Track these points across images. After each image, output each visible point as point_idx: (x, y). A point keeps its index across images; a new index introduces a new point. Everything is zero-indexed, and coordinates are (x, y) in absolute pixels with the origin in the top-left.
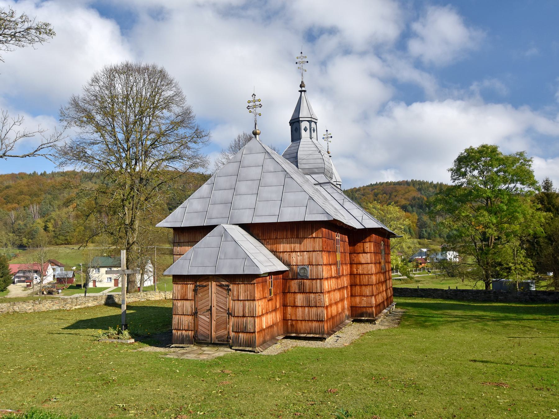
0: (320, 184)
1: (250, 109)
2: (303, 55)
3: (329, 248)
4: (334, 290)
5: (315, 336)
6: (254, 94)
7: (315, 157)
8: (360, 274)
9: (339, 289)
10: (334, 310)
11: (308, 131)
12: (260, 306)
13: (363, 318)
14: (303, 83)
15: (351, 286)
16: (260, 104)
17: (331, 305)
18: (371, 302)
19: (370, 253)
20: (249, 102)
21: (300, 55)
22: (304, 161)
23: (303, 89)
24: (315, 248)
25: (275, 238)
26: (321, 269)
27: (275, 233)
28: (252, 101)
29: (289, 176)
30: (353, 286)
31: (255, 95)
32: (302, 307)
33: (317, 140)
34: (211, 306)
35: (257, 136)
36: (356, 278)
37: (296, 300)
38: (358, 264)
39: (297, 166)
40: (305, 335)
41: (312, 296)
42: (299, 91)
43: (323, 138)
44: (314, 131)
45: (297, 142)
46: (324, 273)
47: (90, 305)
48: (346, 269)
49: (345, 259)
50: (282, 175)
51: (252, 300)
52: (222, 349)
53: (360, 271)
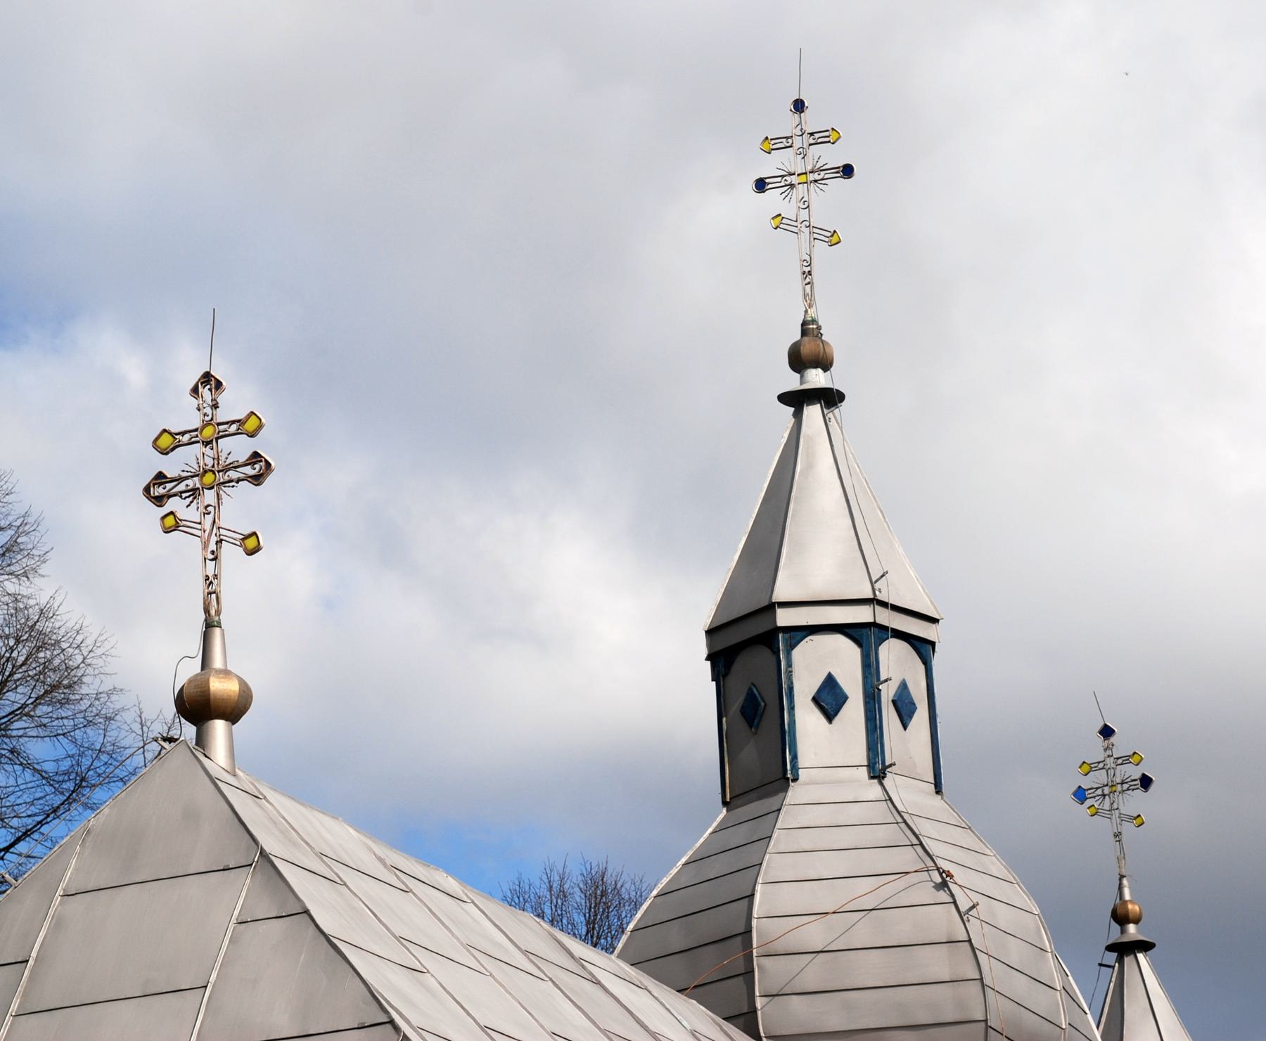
1: (173, 504)
2: (812, 120)
6: (207, 378)
7: (901, 927)
11: (854, 710)
14: (818, 334)
16: (256, 456)
20: (166, 441)
21: (787, 123)
22: (813, 974)
23: (817, 379)
28: (194, 437)
31: (219, 384)
33: (938, 790)
42: (786, 398)
44: (904, 709)
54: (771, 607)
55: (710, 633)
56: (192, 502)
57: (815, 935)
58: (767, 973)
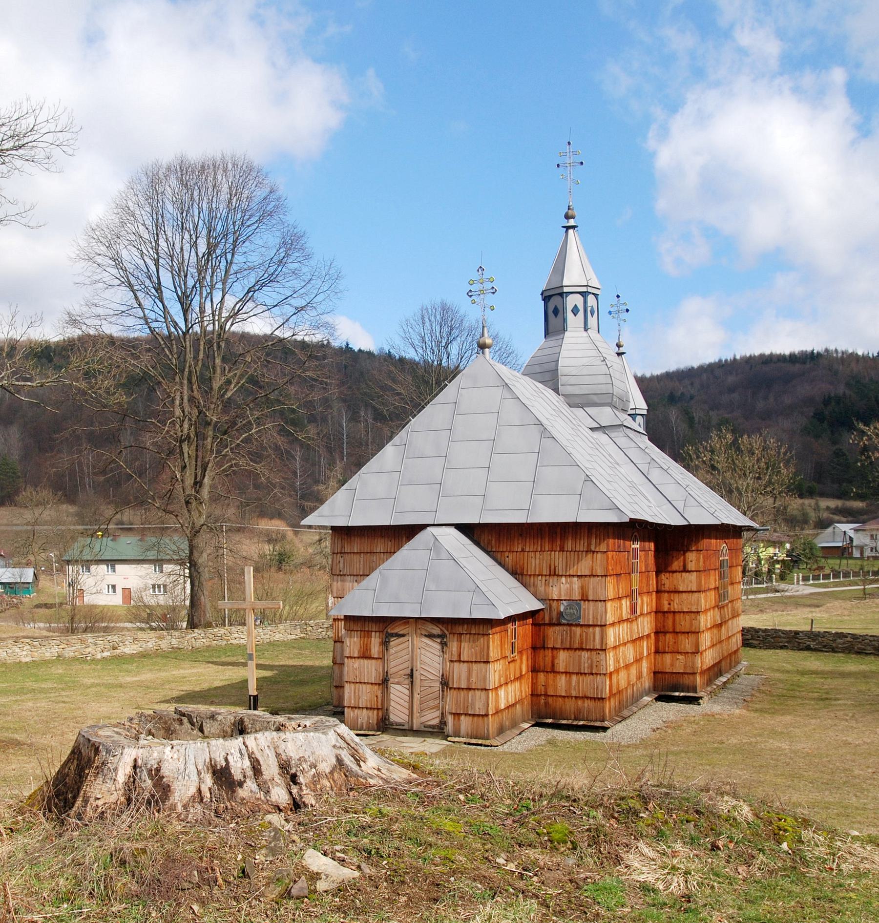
0: (601, 428)
1: (473, 298)
3: (618, 568)
4: (625, 644)
5: (589, 724)
8: (674, 612)
9: (634, 641)
10: (622, 679)
11: (581, 313)
12: (495, 672)
13: (677, 694)
15: (657, 633)
17: (617, 671)
18: (693, 663)
19: (696, 571)
20: (471, 282)
22: (573, 380)
23: (572, 222)
24: (594, 571)
25: (520, 549)
26: (603, 608)
27: (520, 542)
29: (548, 435)
30: (660, 634)
32: (566, 673)
34: (412, 670)
35: (487, 350)
36: (668, 618)
37: (556, 661)
38: (672, 592)
39: (556, 390)
40: (570, 722)
41: (585, 655)
43: (610, 313)
45: (558, 337)
46: (609, 615)
47: (127, 650)
48: (646, 603)
49: (648, 585)
50: (535, 431)
51: (484, 662)
52: (430, 740)
53: (676, 607)
58: (562, 380)
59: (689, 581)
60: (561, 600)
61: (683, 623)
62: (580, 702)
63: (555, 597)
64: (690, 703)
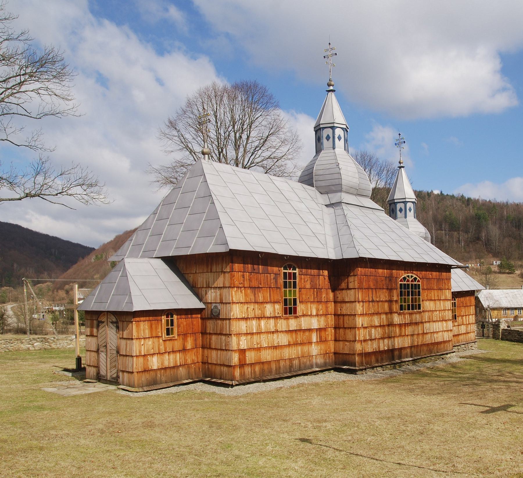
8: (343, 315)
11: (331, 139)
13: (345, 367)
22: (321, 178)
37: (211, 342)
53: (344, 312)
54: (320, 125)
55: (314, 128)
56: (44, 195)
57: (321, 172)
59: (350, 295)
60: (212, 303)
61: (348, 321)
62: (222, 368)
63: (210, 302)
64: (352, 373)
